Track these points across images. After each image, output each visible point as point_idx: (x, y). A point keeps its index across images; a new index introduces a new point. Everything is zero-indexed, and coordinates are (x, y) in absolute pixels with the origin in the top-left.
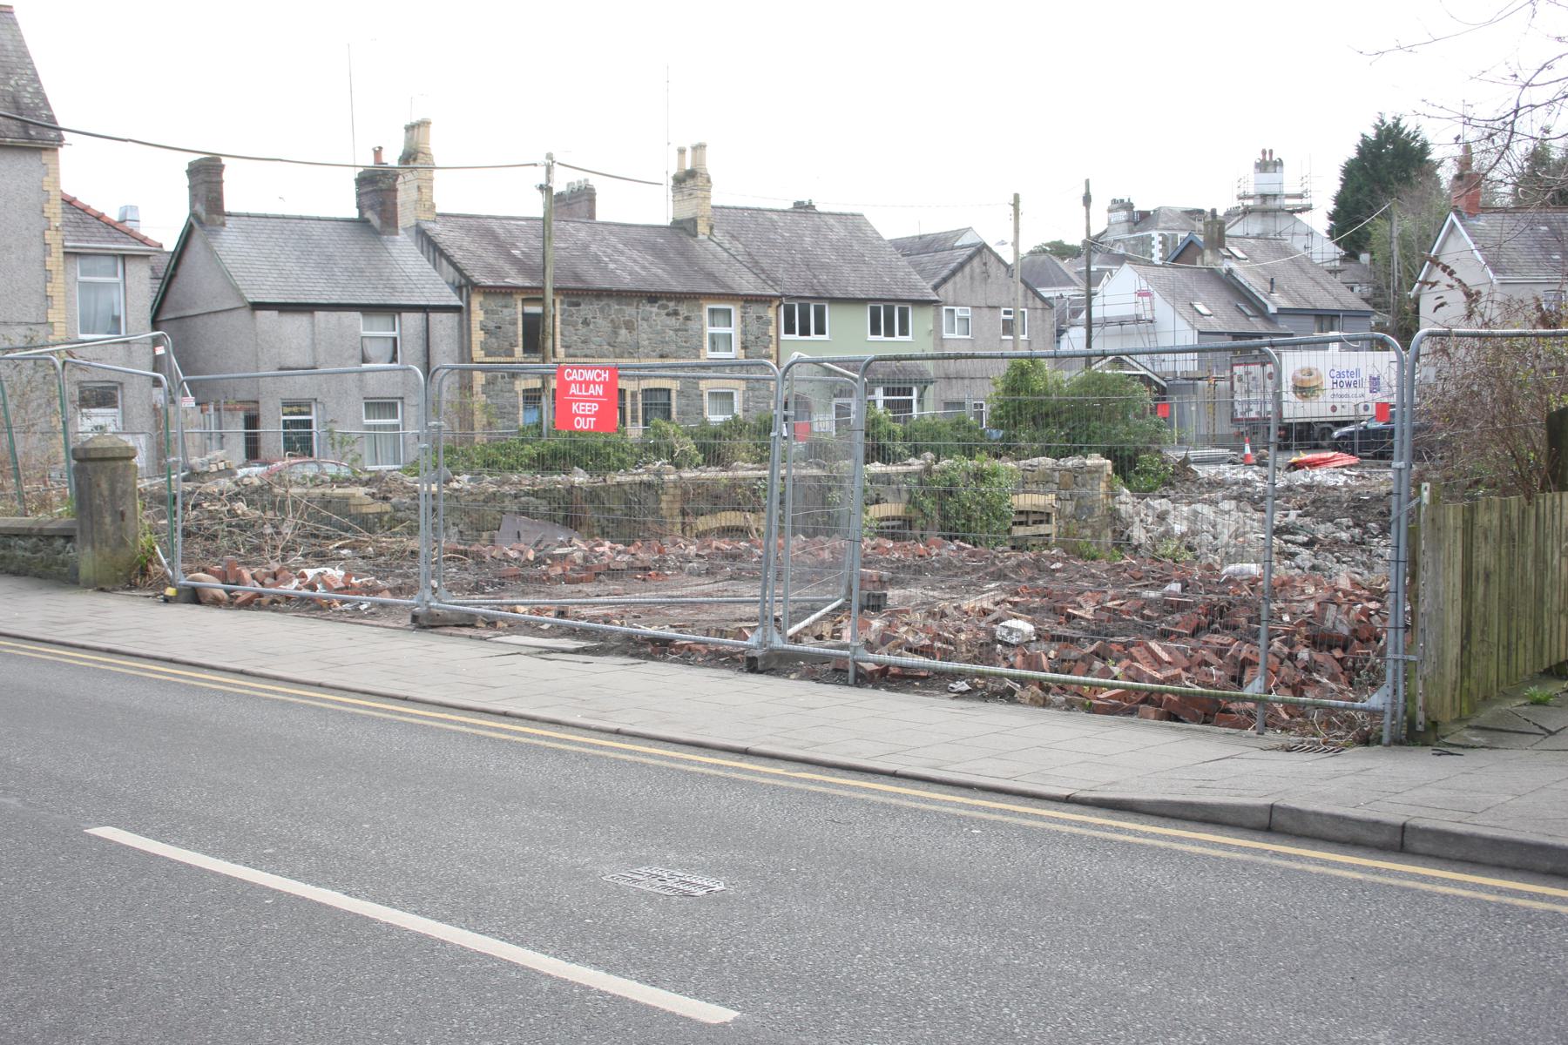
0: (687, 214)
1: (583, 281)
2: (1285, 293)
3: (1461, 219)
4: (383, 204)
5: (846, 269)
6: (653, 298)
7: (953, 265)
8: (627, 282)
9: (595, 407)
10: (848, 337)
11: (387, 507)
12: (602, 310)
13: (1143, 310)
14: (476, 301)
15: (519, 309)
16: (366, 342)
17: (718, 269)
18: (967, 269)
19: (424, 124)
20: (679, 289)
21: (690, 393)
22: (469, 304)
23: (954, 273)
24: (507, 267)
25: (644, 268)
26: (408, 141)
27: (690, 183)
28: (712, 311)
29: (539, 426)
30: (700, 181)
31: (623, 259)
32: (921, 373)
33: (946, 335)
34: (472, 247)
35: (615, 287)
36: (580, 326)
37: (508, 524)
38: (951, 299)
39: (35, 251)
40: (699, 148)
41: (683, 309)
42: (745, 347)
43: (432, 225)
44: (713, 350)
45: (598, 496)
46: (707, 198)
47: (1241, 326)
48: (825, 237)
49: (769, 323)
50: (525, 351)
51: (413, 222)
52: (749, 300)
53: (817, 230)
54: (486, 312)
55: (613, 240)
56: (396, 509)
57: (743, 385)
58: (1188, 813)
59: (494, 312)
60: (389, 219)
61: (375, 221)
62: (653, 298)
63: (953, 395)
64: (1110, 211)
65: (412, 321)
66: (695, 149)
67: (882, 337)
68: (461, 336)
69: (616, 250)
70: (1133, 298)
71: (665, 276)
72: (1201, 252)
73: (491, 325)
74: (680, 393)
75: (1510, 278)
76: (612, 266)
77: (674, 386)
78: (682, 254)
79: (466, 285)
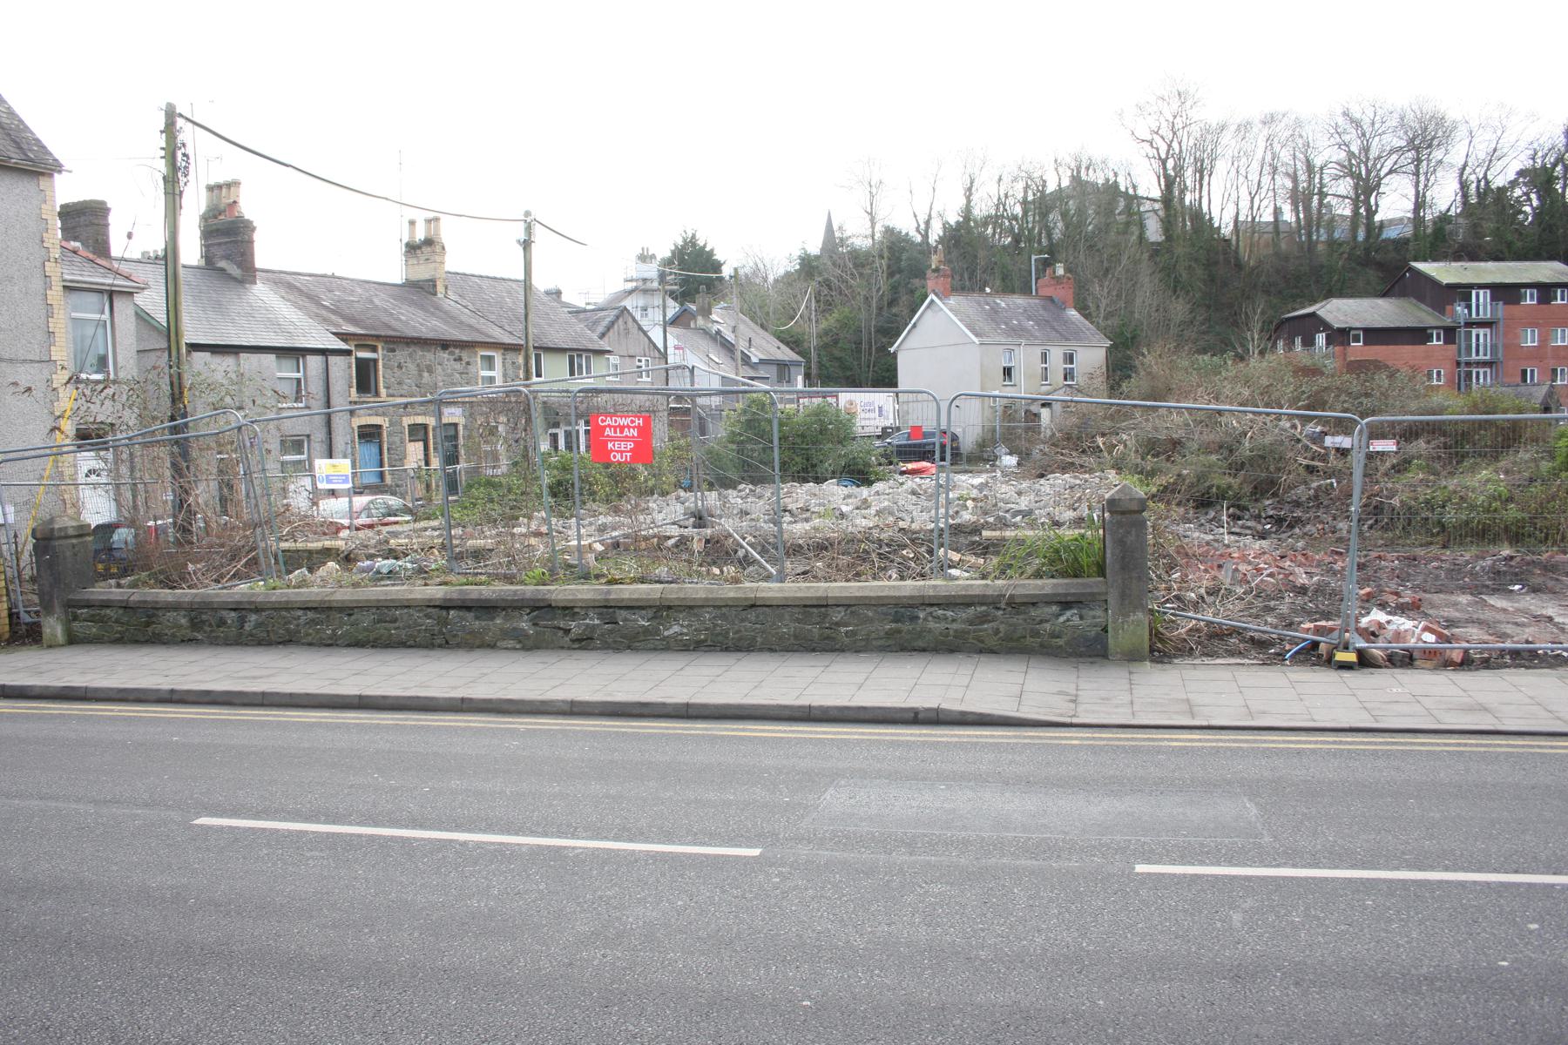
9: (630, 445)
10: (493, 376)
12: (410, 355)
19: (232, 185)
26: (210, 200)
30: (438, 249)
39: (37, 284)
41: (465, 355)
52: (507, 348)
58: (645, 711)
60: (247, 272)
62: (445, 345)
65: (314, 362)
72: (694, 317)
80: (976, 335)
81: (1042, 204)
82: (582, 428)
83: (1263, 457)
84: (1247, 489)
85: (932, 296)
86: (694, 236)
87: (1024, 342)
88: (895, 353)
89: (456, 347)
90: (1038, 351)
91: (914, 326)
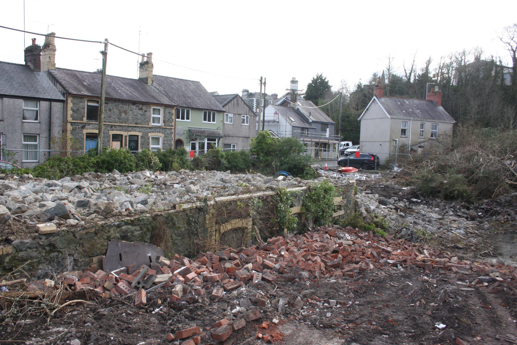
0: (144, 76)
1: (110, 95)
2: (313, 116)
3: (377, 98)
4: (35, 60)
5: (196, 99)
6: (134, 103)
7: (228, 100)
8: (125, 97)
10: (196, 121)
11: (9, 249)
12: (116, 106)
13: (276, 118)
14: (70, 100)
15: (86, 104)
16: (25, 111)
17: (156, 95)
18: (232, 102)
20: (143, 100)
21: (145, 137)
22: (67, 100)
23: (228, 103)
24: (82, 88)
25: (130, 92)
27: (146, 66)
28: (154, 109)
29: (97, 149)
30: (150, 65)
31: (123, 89)
32: (219, 134)
33: (225, 122)
34: (69, 80)
35: (121, 98)
36: (108, 111)
37: (113, 249)
38: (227, 111)
40: (150, 54)
41: (144, 108)
42: (164, 122)
43: (54, 71)
44: (153, 122)
45: (172, 219)
46: (152, 71)
47: (303, 125)
48: (189, 88)
49: (172, 114)
50: (88, 118)
51: (47, 70)
52: (166, 106)
53: (186, 85)
54: (73, 104)
55: (119, 82)
56: (18, 249)
57: (163, 135)
59: (76, 104)
61: (32, 66)
62: (134, 103)
63: (227, 142)
64: (243, 92)
65: (44, 105)
66: (148, 54)
67: (207, 122)
68: (64, 112)
69: (120, 85)
70: (273, 115)
71: (138, 96)
73: (75, 109)
74: (142, 137)
75: (393, 117)
76: (119, 91)
77: (140, 134)
78: (143, 89)
79: (66, 93)
80: (390, 114)
81: (461, 69)
82: (206, 141)
83: (487, 177)
84: (475, 193)
85: (374, 97)
86: (321, 75)
87: (412, 119)
88: (360, 121)
89: (140, 104)
90: (419, 123)
91: (368, 109)
